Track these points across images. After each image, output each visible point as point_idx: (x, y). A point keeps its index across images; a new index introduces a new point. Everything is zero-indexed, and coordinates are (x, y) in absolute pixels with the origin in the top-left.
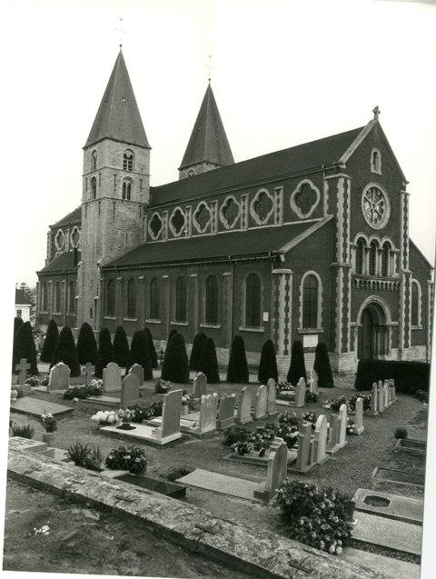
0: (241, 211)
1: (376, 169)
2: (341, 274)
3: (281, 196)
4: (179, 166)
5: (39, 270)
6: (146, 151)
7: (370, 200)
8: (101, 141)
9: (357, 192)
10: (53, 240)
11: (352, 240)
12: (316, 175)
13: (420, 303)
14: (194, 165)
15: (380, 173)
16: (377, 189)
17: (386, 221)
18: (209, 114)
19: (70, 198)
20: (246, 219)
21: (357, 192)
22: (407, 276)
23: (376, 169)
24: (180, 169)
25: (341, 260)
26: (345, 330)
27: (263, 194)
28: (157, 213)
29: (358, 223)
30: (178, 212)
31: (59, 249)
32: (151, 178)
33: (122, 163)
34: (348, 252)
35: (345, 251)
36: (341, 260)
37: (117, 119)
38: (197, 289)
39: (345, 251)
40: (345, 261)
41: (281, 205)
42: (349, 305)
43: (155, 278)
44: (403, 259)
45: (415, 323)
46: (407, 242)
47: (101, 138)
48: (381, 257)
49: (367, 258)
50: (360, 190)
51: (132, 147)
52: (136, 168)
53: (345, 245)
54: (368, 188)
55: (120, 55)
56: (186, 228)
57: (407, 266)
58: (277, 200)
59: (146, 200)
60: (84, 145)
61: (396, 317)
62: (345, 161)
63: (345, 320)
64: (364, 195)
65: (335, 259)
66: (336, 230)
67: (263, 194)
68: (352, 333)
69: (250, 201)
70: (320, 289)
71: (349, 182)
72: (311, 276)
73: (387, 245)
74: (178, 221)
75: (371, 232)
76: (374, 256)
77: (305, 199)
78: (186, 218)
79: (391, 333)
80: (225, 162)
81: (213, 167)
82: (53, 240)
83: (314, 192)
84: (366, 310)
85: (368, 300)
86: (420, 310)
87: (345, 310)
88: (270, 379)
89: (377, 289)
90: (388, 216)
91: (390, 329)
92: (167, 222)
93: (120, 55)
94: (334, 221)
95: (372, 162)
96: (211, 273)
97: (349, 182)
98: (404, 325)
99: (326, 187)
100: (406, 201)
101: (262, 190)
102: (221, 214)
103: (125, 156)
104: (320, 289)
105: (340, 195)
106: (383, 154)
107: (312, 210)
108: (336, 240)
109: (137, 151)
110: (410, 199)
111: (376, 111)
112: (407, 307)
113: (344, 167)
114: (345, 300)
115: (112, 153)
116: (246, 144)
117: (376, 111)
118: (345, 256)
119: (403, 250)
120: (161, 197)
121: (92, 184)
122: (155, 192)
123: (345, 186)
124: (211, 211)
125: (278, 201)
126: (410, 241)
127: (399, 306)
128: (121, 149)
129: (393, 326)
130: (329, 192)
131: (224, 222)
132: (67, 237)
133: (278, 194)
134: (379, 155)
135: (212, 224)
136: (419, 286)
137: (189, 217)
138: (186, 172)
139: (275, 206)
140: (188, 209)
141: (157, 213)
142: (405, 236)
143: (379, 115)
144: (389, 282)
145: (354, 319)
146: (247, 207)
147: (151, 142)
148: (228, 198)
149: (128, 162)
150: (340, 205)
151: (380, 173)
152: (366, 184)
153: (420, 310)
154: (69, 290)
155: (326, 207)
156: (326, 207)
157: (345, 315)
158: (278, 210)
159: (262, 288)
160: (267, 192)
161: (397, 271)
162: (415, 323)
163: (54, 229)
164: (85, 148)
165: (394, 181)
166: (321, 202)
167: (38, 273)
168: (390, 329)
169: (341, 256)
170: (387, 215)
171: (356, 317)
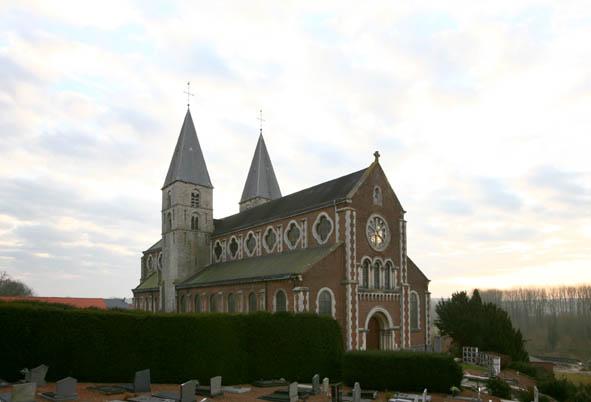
1: (377, 201)
2: (350, 289)
3: (306, 227)
4: (239, 201)
9: (362, 220)
11: (359, 260)
14: (250, 200)
15: (381, 204)
16: (379, 219)
18: (261, 158)
19: (153, 236)
20: (281, 245)
21: (362, 220)
24: (240, 203)
25: (350, 278)
26: (354, 335)
27: (293, 225)
28: (271, 227)
29: (363, 246)
36: (350, 278)
37: (188, 167)
38: (242, 303)
40: (353, 279)
42: (357, 314)
43: (231, 294)
49: (371, 275)
51: (198, 187)
52: (202, 203)
54: (371, 218)
55: (188, 119)
56: (239, 252)
58: (302, 228)
59: (211, 228)
60: (162, 186)
63: (354, 327)
64: (369, 224)
65: (345, 278)
66: (345, 252)
68: (361, 337)
70: (334, 302)
71: (354, 213)
72: (326, 291)
73: (388, 264)
75: (374, 254)
76: (378, 274)
77: (323, 228)
79: (394, 335)
81: (264, 201)
83: (329, 222)
85: (373, 312)
87: (354, 318)
88: (357, 383)
89: (378, 301)
92: (225, 247)
93: (188, 119)
94: (343, 246)
96: (252, 290)
97: (354, 213)
98: (404, 328)
99: (337, 219)
101: (268, 228)
103: (193, 194)
104: (334, 302)
105: (347, 224)
108: (345, 262)
109: (202, 190)
110: (408, 225)
111: (377, 155)
112: (406, 313)
113: (351, 201)
114: (354, 311)
115: (183, 191)
116: (289, 184)
117: (377, 155)
118: (353, 274)
120: (224, 226)
122: (217, 223)
124: (301, 229)
125: (304, 230)
126: (408, 259)
127: (400, 314)
128: (190, 189)
130: (340, 222)
134: (380, 190)
137: (241, 243)
138: (243, 205)
142: (404, 255)
143: (379, 158)
145: (362, 324)
148: (268, 228)
149: (196, 197)
150: (348, 233)
155: (337, 234)
156: (337, 234)
157: (354, 323)
159: (287, 303)
160: (327, 215)
161: (399, 284)
163: (146, 253)
165: (393, 213)
167: (133, 290)
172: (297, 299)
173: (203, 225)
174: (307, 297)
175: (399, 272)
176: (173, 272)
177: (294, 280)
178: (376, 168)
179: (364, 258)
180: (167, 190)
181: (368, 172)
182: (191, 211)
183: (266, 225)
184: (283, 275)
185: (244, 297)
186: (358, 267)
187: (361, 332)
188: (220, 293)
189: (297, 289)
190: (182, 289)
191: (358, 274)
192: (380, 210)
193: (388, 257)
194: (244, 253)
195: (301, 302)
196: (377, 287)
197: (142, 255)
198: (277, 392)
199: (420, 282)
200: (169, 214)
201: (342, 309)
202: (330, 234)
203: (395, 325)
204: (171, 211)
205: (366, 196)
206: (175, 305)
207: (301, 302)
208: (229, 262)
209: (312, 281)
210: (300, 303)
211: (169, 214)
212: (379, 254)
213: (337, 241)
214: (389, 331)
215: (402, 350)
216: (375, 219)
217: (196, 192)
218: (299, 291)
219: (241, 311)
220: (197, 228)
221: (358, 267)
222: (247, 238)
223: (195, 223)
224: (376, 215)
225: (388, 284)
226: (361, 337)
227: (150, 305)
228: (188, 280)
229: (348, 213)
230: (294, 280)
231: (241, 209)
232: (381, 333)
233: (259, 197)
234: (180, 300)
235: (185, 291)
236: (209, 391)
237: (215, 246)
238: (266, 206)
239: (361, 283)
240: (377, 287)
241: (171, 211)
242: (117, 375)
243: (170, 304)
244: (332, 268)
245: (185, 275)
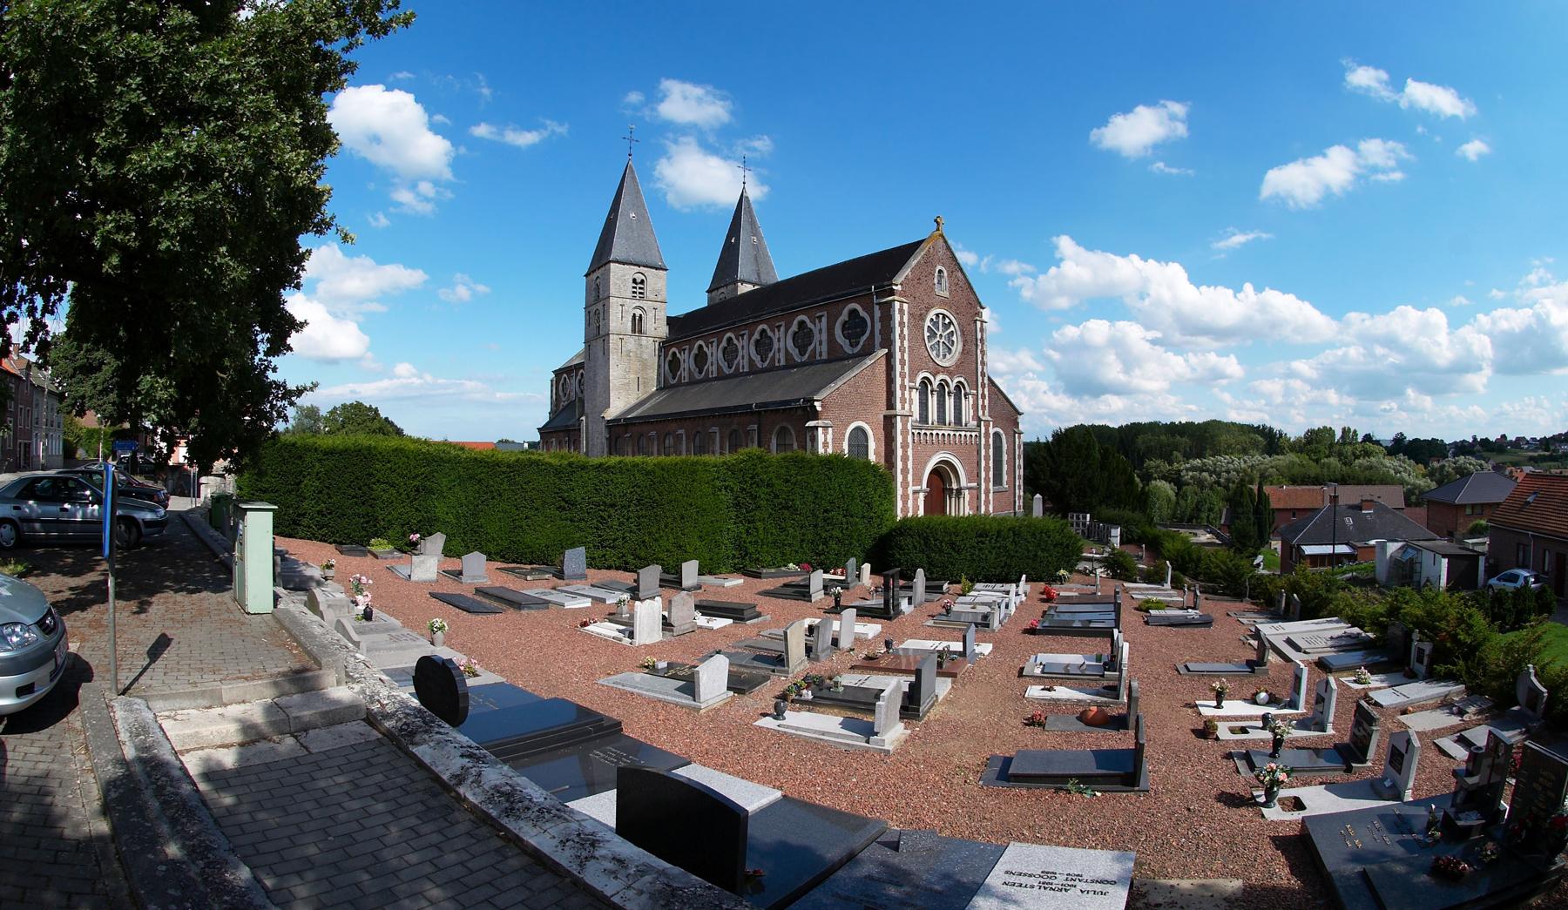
5: (1231, 292)
30: (802, 324)
41: (824, 337)
49: (933, 402)
50: (922, 318)
53: (903, 387)
54: (932, 315)
58: (819, 329)
59: (664, 331)
64: (928, 323)
71: (905, 306)
84: (935, 472)
89: (943, 443)
97: (905, 306)
99: (877, 314)
101: (760, 327)
102: (753, 349)
103: (634, 281)
118: (903, 401)
132: (573, 383)
139: (817, 337)
145: (917, 481)
152: (928, 309)
157: (905, 478)
163: (558, 373)
166: (872, 332)
170: (957, 348)
179: (922, 375)
180: (594, 276)
187: (915, 492)
192: (943, 303)
194: (719, 367)
198: (785, 585)
199: (1007, 413)
212: (945, 370)
217: (639, 277)
226: (916, 500)
231: (710, 299)
239: (916, 416)
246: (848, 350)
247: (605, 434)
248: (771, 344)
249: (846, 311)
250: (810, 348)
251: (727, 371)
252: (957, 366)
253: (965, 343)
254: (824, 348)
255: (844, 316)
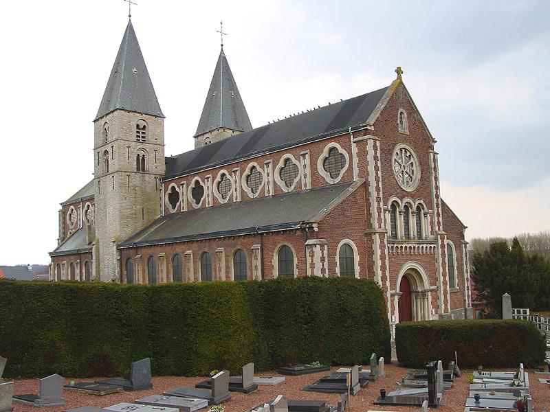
0: (265, 179)
1: (404, 128)
2: (377, 238)
4: (194, 133)
6: (159, 120)
7: (400, 161)
8: (113, 112)
9: (387, 153)
10: (64, 218)
11: (385, 204)
12: (343, 138)
13: (455, 264)
14: (210, 132)
15: (408, 133)
17: (417, 182)
18: (223, 75)
19: (79, 172)
21: (387, 153)
22: (442, 239)
23: (404, 128)
25: (377, 225)
28: (173, 184)
29: (390, 186)
31: (71, 227)
32: (166, 148)
33: (135, 134)
34: (382, 217)
35: (379, 216)
36: (377, 225)
38: (223, 265)
39: (379, 216)
41: (308, 171)
44: (436, 220)
45: (452, 285)
46: (440, 203)
47: (112, 109)
48: (415, 219)
49: (400, 221)
50: (390, 152)
52: (149, 137)
53: (379, 209)
54: (397, 149)
57: (441, 227)
59: (162, 169)
61: (434, 280)
62: (372, 123)
64: (394, 157)
65: (370, 226)
66: (368, 194)
67: (333, 149)
69: (274, 167)
70: (357, 258)
74: (198, 192)
75: (403, 195)
78: (180, 195)
80: (246, 131)
82: (64, 218)
86: (456, 272)
89: (410, 256)
90: (419, 176)
91: (429, 294)
92: (185, 193)
93: (130, 33)
94: (366, 185)
95: (399, 122)
96: (238, 247)
100: (435, 161)
101: (251, 165)
102: (244, 182)
103: (138, 126)
106: (409, 114)
107: (341, 175)
108: (369, 205)
110: (439, 157)
111: (399, 71)
113: (372, 128)
114: (383, 268)
115: (122, 123)
116: (265, 107)
117: (399, 71)
118: (379, 220)
119: (436, 211)
120: (176, 168)
121: (102, 157)
122: (170, 162)
123: (375, 147)
126: (442, 200)
128: (135, 119)
129: (431, 291)
130: (359, 155)
131: (248, 190)
133: (304, 158)
134: (405, 115)
135: (234, 193)
136: (453, 247)
137: (210, 187)
140: (235, 172)
141: (255, 164)
142: (437, 197)
144: (425, 246)
145: (393, 287)
146: (210, 188)
147: (165, 111)
148: (251, 165)
150: (371, 168)
151: (408, 133)
152: (394, 145)
153: (456, 272)
154: (84, 271)
155: (356, 171)
156: (356, 171)
158: (268, 183)
159: (296, 261)
162: (452, 285)
163: (65, 206)
164: (94, 121)
165: (423, 141)
167: (50, 254)
168: (429, 294)
169: (376, 221)
170: (417, 175)
171: (395, 285)
172: (312, 255)
173: (150, 165)
174: (325, 252)
175: (432, 217)
176: (112, 225)
177: (306, 231)
178: (399, 87)
179: (392, 199)
180: (102, 122)
181: (389, 93)
182: (136, 147)
183: (247, 162)
184: (289, 225)
185: (227, 256)
186: (385, 210)
187: (392, 295)
188: (188, 252)
189: (310, 242)
190: (127, 250)
191: (385, 221)
192: (405, 139)
193: (419, 197)
194: (214, 198)
195: (317, 259)
196: (408, 236)
197: (61, 207)
198: (322, 381)
199: (454, 226)
200: (106, 152)
201: (368, 266)
202: (343, 171)
203: (432, 284)
204: (108, 148)
205: (384, 121)
206: (117, 270)
207: (317, 259)
208: (192, 212)
209: (328, 230)
210: (317, 263)
211: (106, 152)
212: (409, 194)
213: (356, 178)
214: (424, 293)
215: (441, 316)
216: (401, 150)
217: (142, 124)
218: (315, 245)
219: (165, 281)
220: (143, 170)
221: (385, 210)
222: (218, 179)
223: (141, 163)
224: (403, 146)
225: (419, 232)
226: (392, 301)
227: (78, 271)
228: (131, 238)
229: (370, 143)
230: (306, 231)
231: (197, 144)
232: (413, 296)
233: (224, 128)
234: (125, 264)
235: (132, 252)
236: (241, 385)
237: (169, 191)
238: (231, 141)
239: (390, 233)
240: (408, 236)
241: (108, 148)
242: (101, 367)
243: (107, 268)
244: (354, 215)
245: (129, 231)
246: (330, 181)
247: (116, 256)
248: (261, 177)
249: (326, 150)
250: (296, 180)
251: (222, 201)
252: (417, 190)
253: (422, 171)
254: (309, 180)
255: (325, 153)
